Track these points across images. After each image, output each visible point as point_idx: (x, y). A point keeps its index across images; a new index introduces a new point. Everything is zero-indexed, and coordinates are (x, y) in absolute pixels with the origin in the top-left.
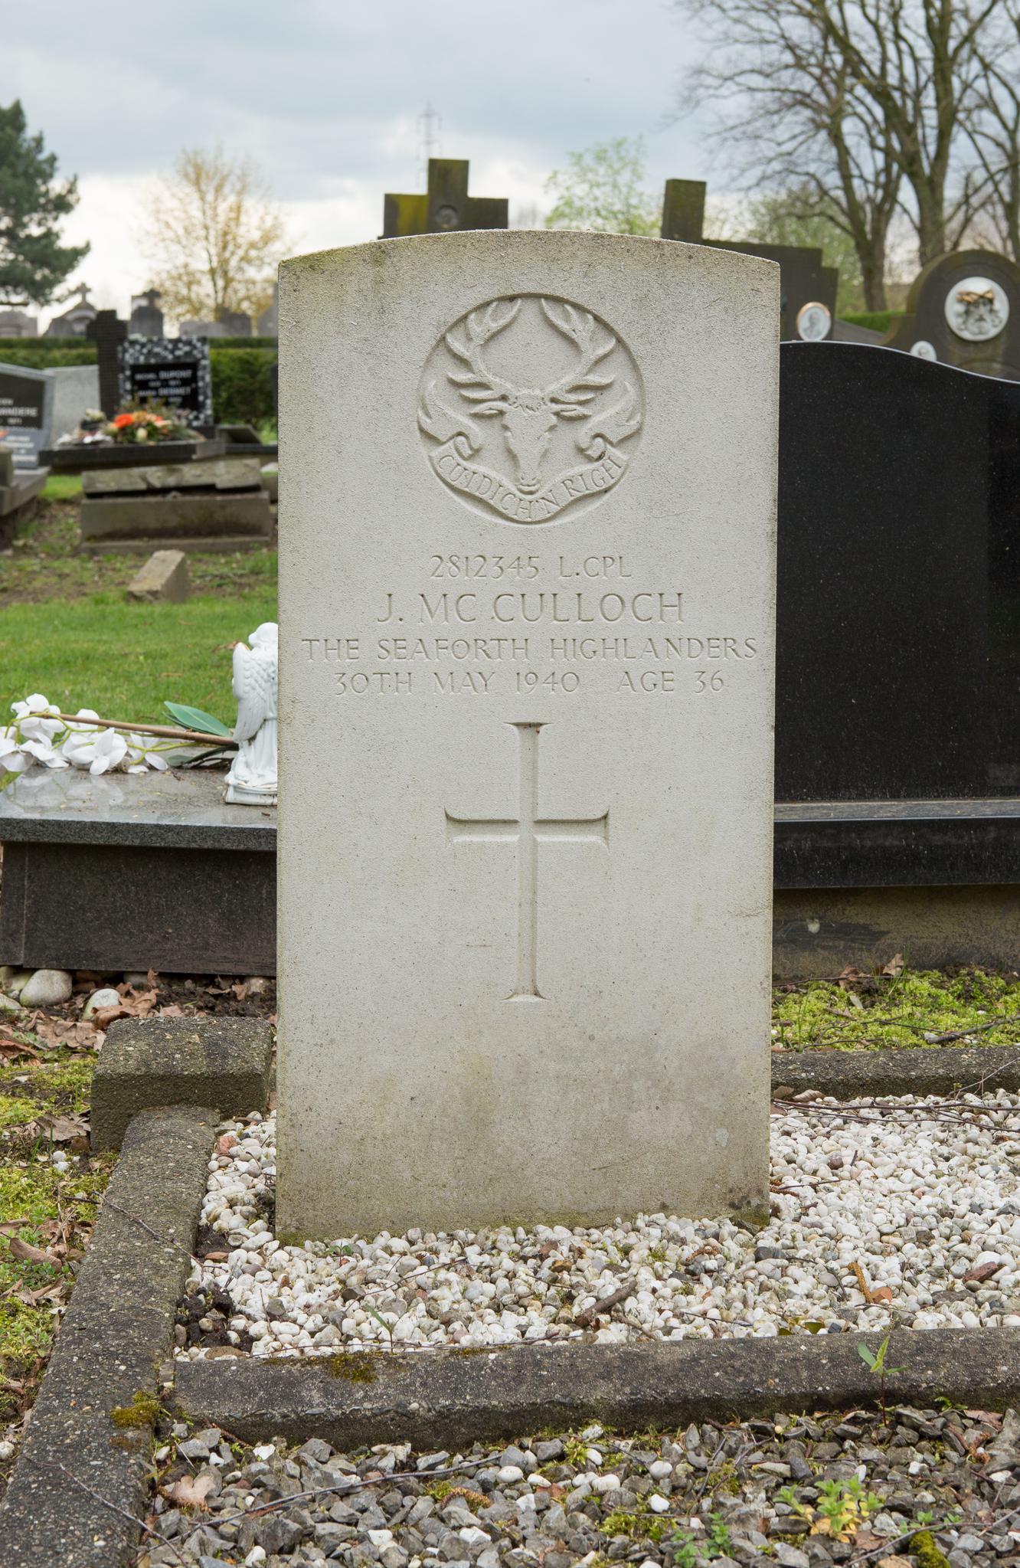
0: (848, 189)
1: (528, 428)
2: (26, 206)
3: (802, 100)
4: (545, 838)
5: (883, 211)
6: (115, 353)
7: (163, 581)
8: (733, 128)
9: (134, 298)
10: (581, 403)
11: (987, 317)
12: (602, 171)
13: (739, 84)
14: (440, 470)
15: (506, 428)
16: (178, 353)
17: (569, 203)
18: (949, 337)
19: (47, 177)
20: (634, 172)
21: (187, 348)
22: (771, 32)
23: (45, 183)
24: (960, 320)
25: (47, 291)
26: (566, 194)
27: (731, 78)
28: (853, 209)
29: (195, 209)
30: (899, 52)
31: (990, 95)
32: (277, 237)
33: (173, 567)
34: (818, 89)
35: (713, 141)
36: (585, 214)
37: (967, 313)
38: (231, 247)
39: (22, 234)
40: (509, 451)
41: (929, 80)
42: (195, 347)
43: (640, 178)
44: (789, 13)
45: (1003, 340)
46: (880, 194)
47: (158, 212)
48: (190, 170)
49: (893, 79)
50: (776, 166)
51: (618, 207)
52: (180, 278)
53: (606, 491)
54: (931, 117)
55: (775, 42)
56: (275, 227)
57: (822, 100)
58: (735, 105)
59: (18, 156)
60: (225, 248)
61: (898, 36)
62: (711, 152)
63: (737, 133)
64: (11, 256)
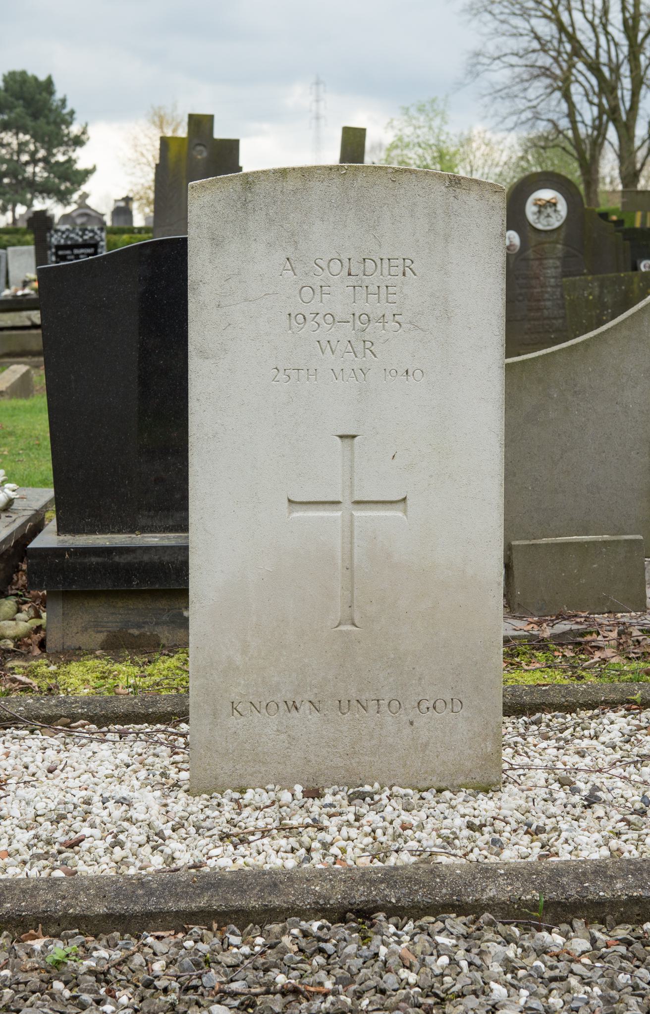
0: (575, 129)
2: (55, 142)
3: (545, 72)
4: (360, 514)
5: (598, 142)
6: (46, 237)
7: (8, 385)
8: (500, 90)
9: (116, 201)
11: (553, 214)
12: (422, 118)
13: (504, 62)
16: (86, 237)
17: (400, 139)
18: (528, 228)
19: (69, 124)
20: (443, 119)
21: (91, 235)
22: (524, 29)
23: (67, 127)
24: (535, 217)
25: (68, 197)
26: (399, 133)
27: (499, 58)
28: (577, 141)
30: (608, 41)
33: (18, 376)
34: (555, 65)
35: (487, 99)
36: (411, 146)
37: (540, 212)
39: (53, 160)
41: (625, 57)
42: (96, 234)
43: (446, 123)
44: (536, 16)
45: (563, 229)
46: (595, 133)
47: (136, 146)
48: (156, 119)
49: (603, 58)
51: (432, 141)
54: (627, 83)
55: (527, 35)
57: (558, 72)
58: (501, 75)
59: (50, 110)
61: (607, 33)
62: (486, 106)
63: (503, 93)
64: (46, 175)
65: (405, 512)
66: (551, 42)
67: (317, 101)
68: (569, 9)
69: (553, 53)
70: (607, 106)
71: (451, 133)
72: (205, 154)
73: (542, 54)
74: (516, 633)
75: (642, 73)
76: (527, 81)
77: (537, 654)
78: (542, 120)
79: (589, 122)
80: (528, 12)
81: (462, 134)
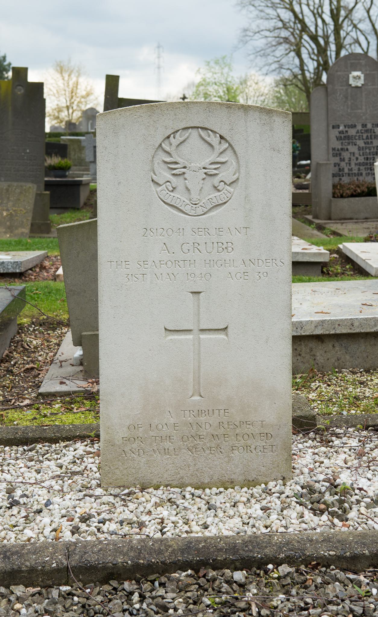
0: (303, 74)
1: (194, 180)
3: (286, 40)
10: (215, 169)
13: (261, 35)
14: (160, 195)
15: (186, 179)
17: (204, 80)
20: (229, 68)
22: (273, 15)
23: (7, 73)
26: (204, 77)
27: (258, 32)
28: (305, 81)
29: (61, 83)
31: (358, 38)
32: (92, 94)
35: (252, 57)
36: (211, 84)
38: (74, 98)
40: (187, 188)
41: (332, 32)
43: (231, 71)
48: (58, 68)
49: (320, 33)
50: (274, 66)
51: (223, 82)
52: (55, 109)
53: (225, 203)
54: (333, 47)
56: (91, 90)
57: (293, 40)
58: (260, 42)
60: (72, 97)
65: (227, 335)
66: (289, 23)
67: (159, 57)
68: (300, 4)
69: (291, 30)
70: (322, 62)
71: (235, 75)
72: (22, 91)
73: (283, 29)
74: (77, 389)
75: (342, 41)
76: (275, 46)
77: (85, 401)
78: (284, 69)
79: (312, 70)
80: (276, 5)
81: (241, 77)
